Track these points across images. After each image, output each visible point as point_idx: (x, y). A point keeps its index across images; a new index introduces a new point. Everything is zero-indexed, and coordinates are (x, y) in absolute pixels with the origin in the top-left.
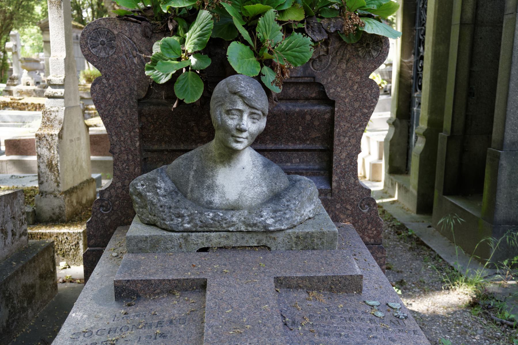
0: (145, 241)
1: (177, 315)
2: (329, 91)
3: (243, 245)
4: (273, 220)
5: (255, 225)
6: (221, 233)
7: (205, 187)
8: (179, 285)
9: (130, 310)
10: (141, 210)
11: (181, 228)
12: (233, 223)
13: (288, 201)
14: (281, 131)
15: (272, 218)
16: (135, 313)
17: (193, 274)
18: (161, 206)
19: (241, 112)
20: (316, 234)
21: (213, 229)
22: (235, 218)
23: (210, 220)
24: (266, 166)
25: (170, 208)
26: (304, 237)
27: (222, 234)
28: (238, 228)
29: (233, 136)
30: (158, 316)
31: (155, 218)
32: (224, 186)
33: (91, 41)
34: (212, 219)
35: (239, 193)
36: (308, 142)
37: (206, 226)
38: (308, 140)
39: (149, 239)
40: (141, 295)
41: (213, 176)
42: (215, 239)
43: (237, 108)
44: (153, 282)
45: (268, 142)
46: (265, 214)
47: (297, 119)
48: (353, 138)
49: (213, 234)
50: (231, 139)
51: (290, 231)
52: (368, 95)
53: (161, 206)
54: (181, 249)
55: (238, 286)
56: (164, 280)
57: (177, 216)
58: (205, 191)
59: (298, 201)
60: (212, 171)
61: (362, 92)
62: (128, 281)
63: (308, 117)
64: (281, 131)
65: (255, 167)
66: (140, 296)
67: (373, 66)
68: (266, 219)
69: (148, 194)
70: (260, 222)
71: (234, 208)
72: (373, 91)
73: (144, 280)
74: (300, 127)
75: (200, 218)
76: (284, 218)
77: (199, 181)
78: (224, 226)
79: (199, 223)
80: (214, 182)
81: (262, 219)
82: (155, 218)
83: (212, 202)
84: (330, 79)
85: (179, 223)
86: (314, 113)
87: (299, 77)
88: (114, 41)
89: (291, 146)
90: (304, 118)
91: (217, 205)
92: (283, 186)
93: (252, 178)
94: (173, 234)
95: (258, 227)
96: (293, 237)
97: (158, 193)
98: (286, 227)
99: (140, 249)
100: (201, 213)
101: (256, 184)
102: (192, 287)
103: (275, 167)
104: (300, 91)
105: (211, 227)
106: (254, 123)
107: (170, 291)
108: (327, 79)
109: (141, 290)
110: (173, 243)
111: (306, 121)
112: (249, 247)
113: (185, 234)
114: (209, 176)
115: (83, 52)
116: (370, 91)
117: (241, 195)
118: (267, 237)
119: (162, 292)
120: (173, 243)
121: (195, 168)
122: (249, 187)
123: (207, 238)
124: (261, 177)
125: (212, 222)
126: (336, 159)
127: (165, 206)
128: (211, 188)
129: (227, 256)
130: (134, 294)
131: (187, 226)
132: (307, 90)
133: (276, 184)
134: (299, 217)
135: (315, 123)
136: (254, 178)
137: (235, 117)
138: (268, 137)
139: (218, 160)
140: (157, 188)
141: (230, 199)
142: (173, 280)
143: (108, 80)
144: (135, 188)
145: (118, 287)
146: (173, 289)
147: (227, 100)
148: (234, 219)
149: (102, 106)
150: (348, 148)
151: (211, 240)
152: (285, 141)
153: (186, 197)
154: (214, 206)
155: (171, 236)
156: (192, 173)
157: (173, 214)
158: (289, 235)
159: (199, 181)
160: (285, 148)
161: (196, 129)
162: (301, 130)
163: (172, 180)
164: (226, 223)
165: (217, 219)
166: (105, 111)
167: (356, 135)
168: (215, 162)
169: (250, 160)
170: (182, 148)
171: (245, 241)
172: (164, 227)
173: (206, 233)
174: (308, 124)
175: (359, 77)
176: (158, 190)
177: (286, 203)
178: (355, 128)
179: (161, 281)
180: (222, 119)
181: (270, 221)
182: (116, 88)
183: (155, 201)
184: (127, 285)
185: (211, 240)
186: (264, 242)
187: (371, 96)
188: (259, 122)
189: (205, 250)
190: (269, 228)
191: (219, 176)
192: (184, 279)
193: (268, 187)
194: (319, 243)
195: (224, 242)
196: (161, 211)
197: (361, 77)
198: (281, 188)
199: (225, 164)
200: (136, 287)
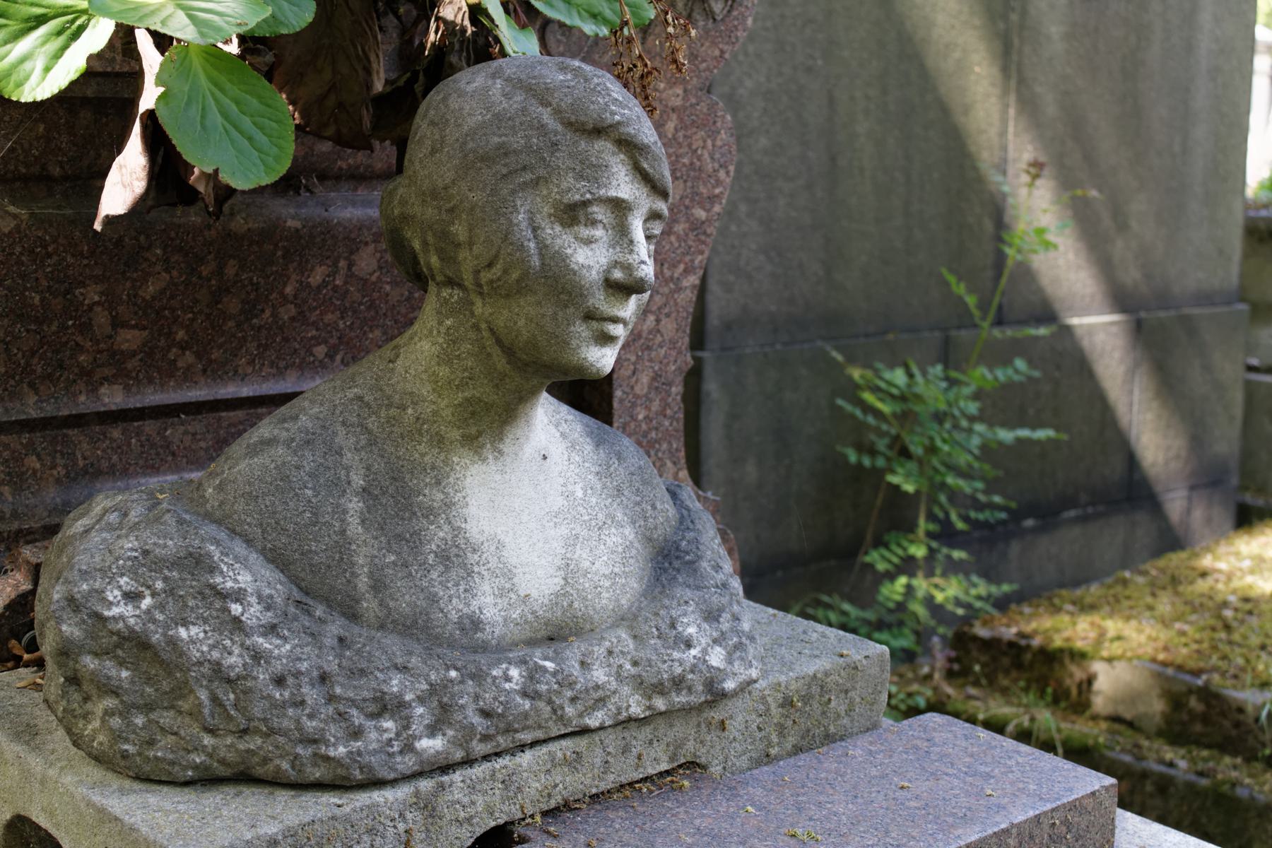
5: (678, 683)
6: (554, 747)
7: (431, 558)
10: (139, 721)
11: (407, 763)
18: (280, 681)
19: (620, 207)
20: (835, 677)
21: (527, 737)
23: (519, 699)
25: (324, 678)
29: (590, 316)
31: (254, 743)
32: (500, 546)
34: (525, 694)
35: (558, 562)
37: (509, 730)
41: (449, 505)
43: (612, 193)
46: (692, 630)
48: (668, 315)
49: (526, 758)
50: (581, 329)
52: (706, 156)
53: (280, 681)
57: (372, 708)
58: (434, 575)
60: (438, 483)
61: (690, 146)
67: (717, 53)
69: (183, 633)
71: (557, 632)
72: (719, 143)
75: (477, 697)
77: (400, 537)
78: (570, 711)
80: (457, 531)
81: (693, 652)
82: (254, 743)
85: (389, 742)
91: (497, 632)
94: (377, 796)
95: (690, 689)
97: (237, 620)
100: (478, 676)
113: (425, 785)
114: (431, 509)
116: (709, 142)
117: (569, 571)
121: (358, 481)
124: (604, 487)
125: (527, 704)
126: (621, 401)
127: (297, 674)
128: (455, 557)
131: (431, 745)
137: (599, 232)
139: (455, 434)
140: (224, 596)
141: (534, 594)
144: (99, 617)
147: (562, 160)
148: (599, 675)
150: (653, 354)
153: (353, 616)
155: (372, 807)
156: (354, 505)
157: (353, 703)
159: (400, 537)
161: (101, 318)
163: (263, 552)
165: (544, 688)
167: (676, 304)
168: (439, 441)
170: (34, 414)
172: (317, 774)
175: (679, 91)
176: (236, 609)
178: (672, 278)
180: (543, 247)
181: (717, 658)
183: (232, 660)
187: (712, 158)
191: (472, 501)
193: (633, 522)
196: (284, 705)
197: (685, 91)
199: (482, 446)
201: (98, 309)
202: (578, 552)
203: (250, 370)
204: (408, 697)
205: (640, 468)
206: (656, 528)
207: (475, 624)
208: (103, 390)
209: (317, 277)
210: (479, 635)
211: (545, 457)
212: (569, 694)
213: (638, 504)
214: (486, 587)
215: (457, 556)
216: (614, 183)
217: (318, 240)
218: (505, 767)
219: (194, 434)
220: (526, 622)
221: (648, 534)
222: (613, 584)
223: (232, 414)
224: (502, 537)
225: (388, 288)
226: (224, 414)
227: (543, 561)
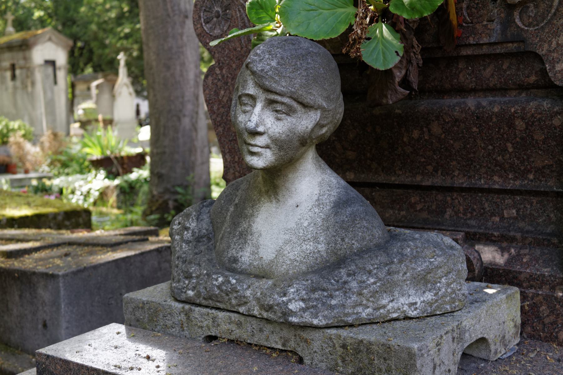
2: (554, 67)
4: (302, 304)
6: (232, 315)
11: (183, 297)
12: (245, 300)
13: (349, 275)
14: (474, 153)
15: (303, 300)
19: (253, 98)
22: (251, 290)
24: (339, 205)
26: (355, 349)
32: (260, 235)
33: (206, 14)
35: (278, 248)
36: (531, 177)
38: (529, 171)
39: (147, 307)
41: (252, 215)
42: (224, 323)
43: (247, 92)
45: (456, 173)
47: (500, 129)
49: (221, 314)
51: (333, 331)
59: (377, 278)
60: (252, 207)
63: (520, 124)
64: (474, 153)
65: (319, 205)
68: (290, 301)
70: (278, 305)
74: (509, 145)
76: (324, 304)
78: (234, 302)
79: (202, 290)
81: (284, 299)
83: (238, 260)
84: (554, 43)
86: (529, 115)
87: (495, 44)
88: (230, 9)
89: (497, 183)
90: (511, 126)
91: (244, 267)
92: (356, 245)
93: (306, 224)
95: (275, 312)
96: (337, 346)
98: (324, 323)
101: (309, 236)
103: (361, 206)
104: (505, 71)
106: (278, 119)
108: (550, 43)
111: (518, 133)
112: (269, 348)
113: (187, 307)
114: (247, 216)
115: (195, 30)
117: (279, 253)
118: (295, 336)
122: (295, 240)
124: (323, 225)
128: (244, 236)
132: (518, 69)
133: (343, 240)
134: (369, 310)
135: (536, 137)
136: (309, 224)
138: (454, 163)
141: (265, 258)
143: (221, 69)
148: (248, 293)
149: (215, 108)
151: (218, 325)
152: (486, 173)
154: (238, 266)
158: (331, 339)
160: (486, 186)
162: (511, 150)
164: (236, 298)
166: (217, 116)
169: (317, 192)
173: (213, 311)
174: (522, 139)
177: (345, 278)
182: (230, 80)
186: (292, 345)
188: (289, 119)
190: (290, 319)
191: (260, 216)
193: (328, 244)
194: (383, 367)
195: (237, 333)
198: (351, 248)
201: (336, 142)
202: (287, 247)
203: (401, 173)
204: (194, 275)
205: (343, 221)
206: (340, 250)
207: (235, 260)
208: (347, 174)
209: (416, 134)
210: (234, 265)
211: (297, 206)
212: (235, 295)
213: (334, 236)
214: (249, 250)
215: (245, 235)
216: (248, 88)
217: (410, 118)
218: (213, 313)
219: (383, 196)
220: (259, 268)
221: (335, 251)
222: (291, 264)
223: (398, 190)
224: (262, 232)
225: (452, 142)
226: (394, 190)
227: (272, 246)
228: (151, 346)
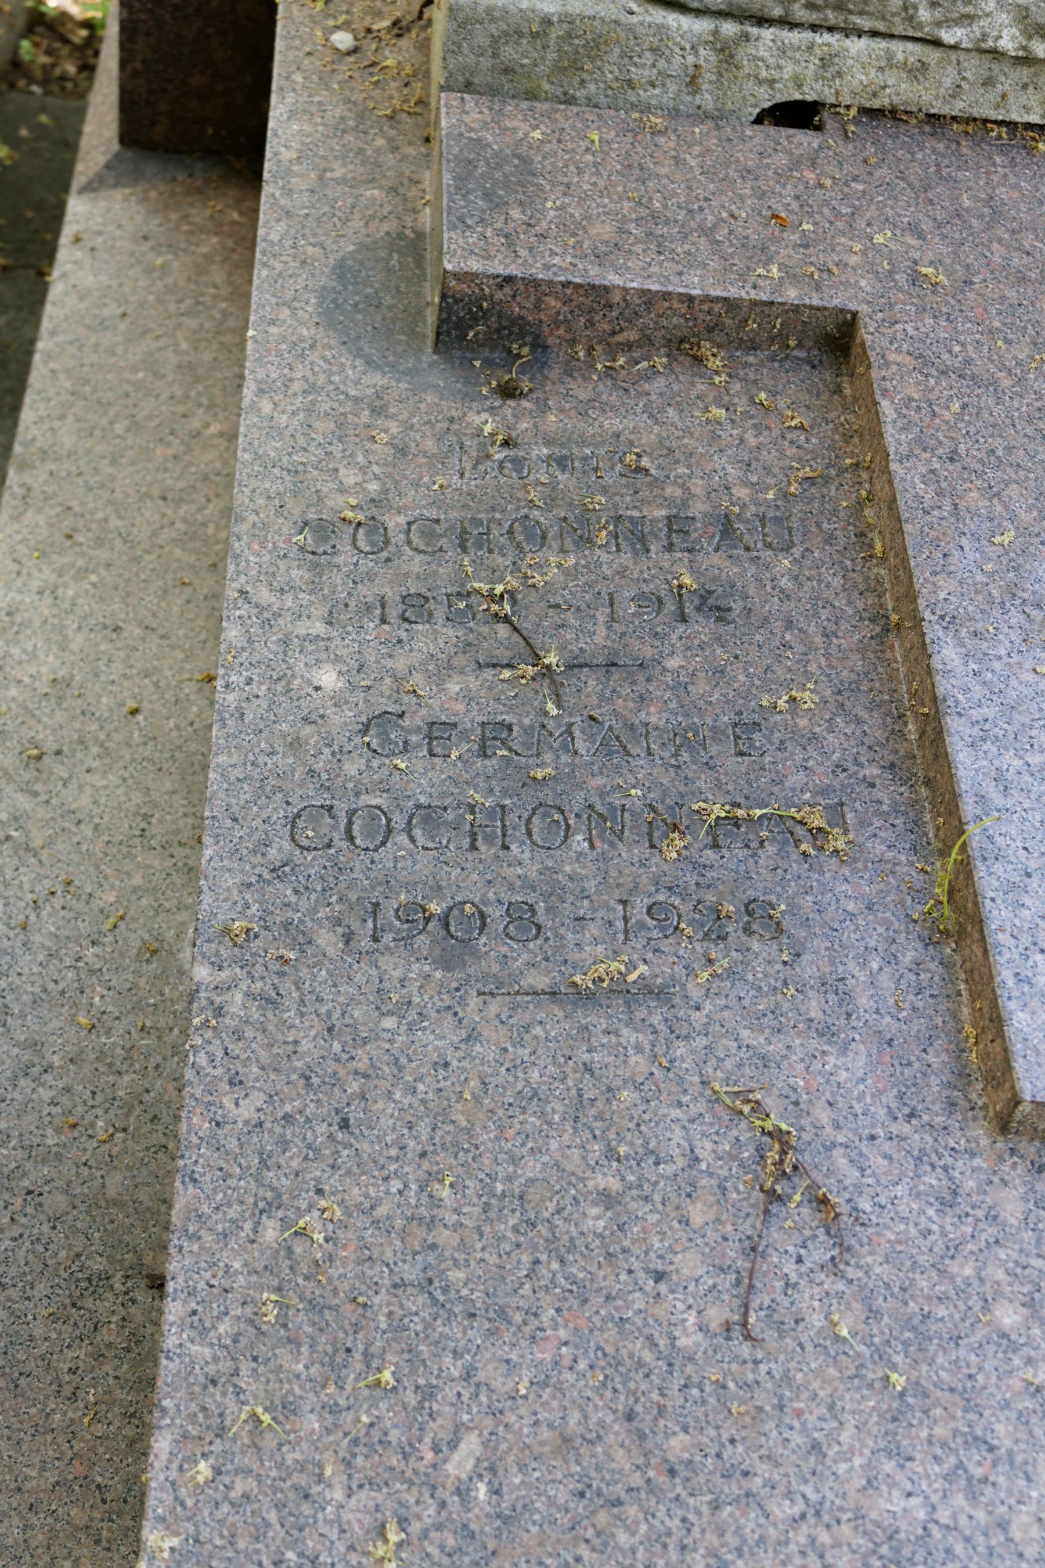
0: (535, 36)
1: (741, 493)
3: (976, 113)
8: (728, 322)
9: (520, 418)
16: (548, 443)
17: (790, 276)
21: (865, 23)
27: (900, 50)
28: (984, 36)
30: (658, 483)
39: (556, 32)
40: (550, 341)
44: (616, 297)
49: (857, 46)
54: (694, 93)
55: (1006, 383)
56: (667, 296)
62: (509, 279)
66: (546, 348)
73: (580, 286)
99: (507, 71)
102: (782, 339)
105: (861, 13)
107: (682, 341)
109: (556, 323)
110: (661, 64)
113: (729, 28)
119: (646, 341)
120: (661, 64)
123: (825, 62)
129: (915, 171)
130: (522, 335)
142: (708, 299)
145: (456, 301)
146: (696, 335)
155: (662, 28)
171: (993, 95)
173: (827, 37)
179: (649, 298)
184: (499, 295)
185: (839, 74)
189: (796, 115)
192: (755, 303)
195: (898, 91)
200: (537, 307)
228: (948, 740)
